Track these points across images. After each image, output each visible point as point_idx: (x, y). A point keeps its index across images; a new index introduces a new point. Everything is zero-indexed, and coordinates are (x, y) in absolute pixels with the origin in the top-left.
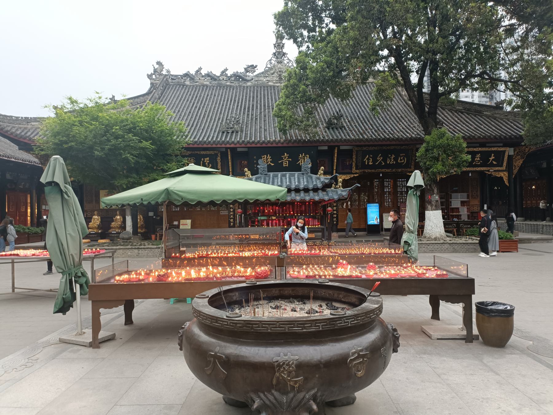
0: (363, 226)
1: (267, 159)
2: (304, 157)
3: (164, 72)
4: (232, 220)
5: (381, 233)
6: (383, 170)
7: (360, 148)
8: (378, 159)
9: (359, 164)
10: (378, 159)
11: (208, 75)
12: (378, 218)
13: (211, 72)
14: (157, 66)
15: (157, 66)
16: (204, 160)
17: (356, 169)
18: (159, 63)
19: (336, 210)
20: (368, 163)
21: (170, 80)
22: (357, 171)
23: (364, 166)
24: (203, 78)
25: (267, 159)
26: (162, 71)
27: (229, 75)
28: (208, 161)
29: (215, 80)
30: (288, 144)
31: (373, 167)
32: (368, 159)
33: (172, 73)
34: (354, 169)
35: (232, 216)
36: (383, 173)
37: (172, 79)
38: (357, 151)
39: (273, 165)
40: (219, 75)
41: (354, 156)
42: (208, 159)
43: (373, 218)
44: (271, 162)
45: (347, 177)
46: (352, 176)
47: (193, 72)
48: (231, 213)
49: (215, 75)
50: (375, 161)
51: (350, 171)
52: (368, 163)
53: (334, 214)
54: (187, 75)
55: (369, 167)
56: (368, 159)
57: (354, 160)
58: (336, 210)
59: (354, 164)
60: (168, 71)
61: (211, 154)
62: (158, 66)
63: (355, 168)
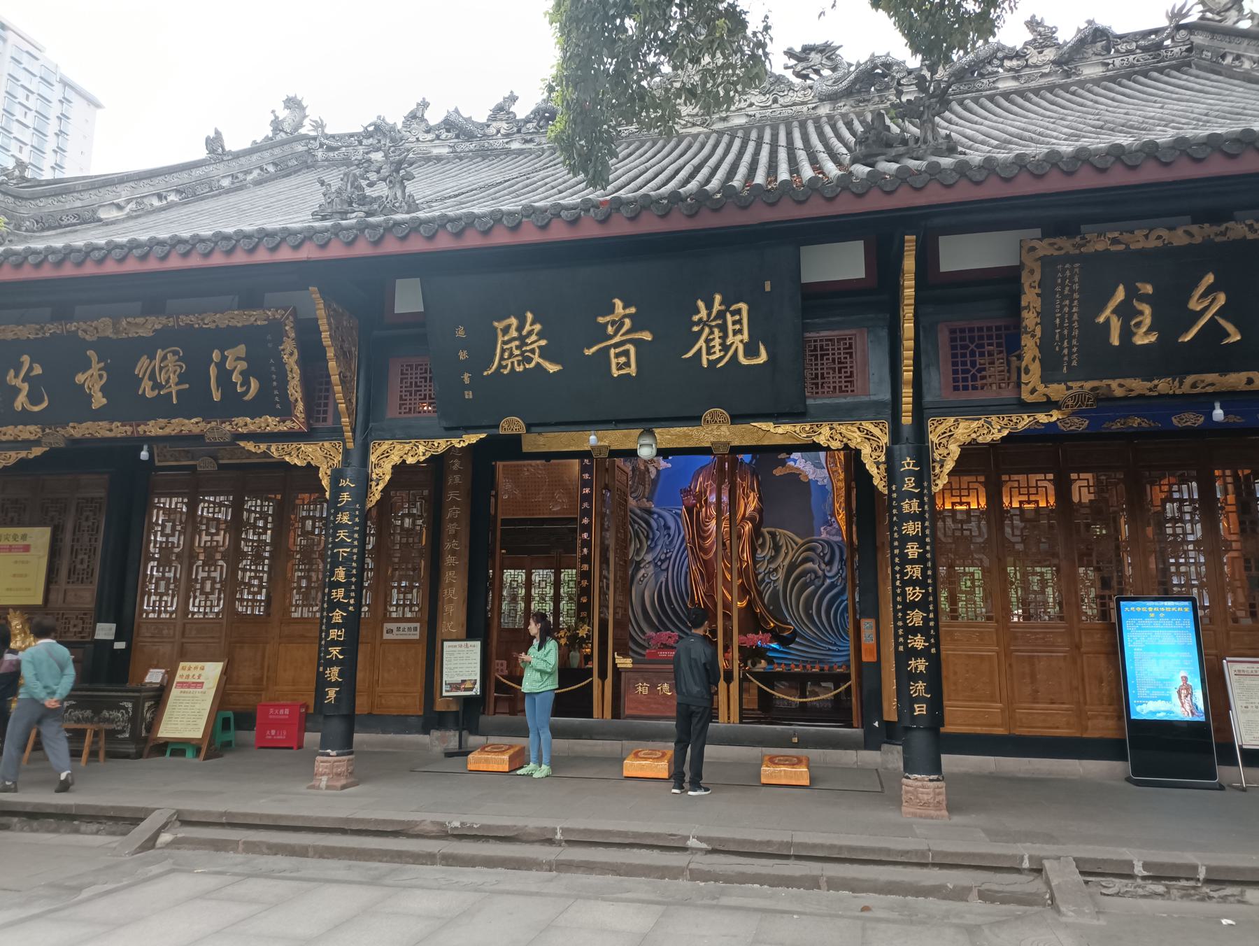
0: (1101, 727)
1: (522, 339)
2: (721, 315)
3: (306, 130)
4: (334, 673)
5: (1224, 773)
6: (1236, 380)
7: (1066, 245)
8: (1194, 305)
9: (1070, 351)
10: (1194, 305)
11: (448, 124)
12: (1196, 682)
13: (457, 111)
14: (283, 114)
15: (283, 114)
16: (224, 358)
17: (1045, 380)
18: (293, 103)
19: (923, 630)
20: (1127, 334)
21: (320, 154)
22: (1057, 391)
23: (1101, 358)
24: (430, 136)
25: (522, 339)
26: (300, 125)
27: (521, 115)
28: (243, 365)
29: (470, 137)
30: (604, 222)
31: (1167, 358)
32: (1127, 312)
33: (329, 131)
34: (1033, 377)
35: (335, 651)
36: (1229, 398)
37: (330, 149)
38: (1046, 262)
39: (552, 368)
40: (483, 120)
41: (1030, 297)
42: (241, 350)
43: (1163, 684)
44: (544, 353)
45: (994, 430)
46: (1024, 422)
47: (396, 118)
48: (334, 633)
49: (469, 120)
50: (1172, 315)
51: (1008, 394)
52: (1127, 334)
53: (915, 653)
54: (379, 130)
55: (1130, 360)
56: (1127, 312)
57: (1030, 319)
58: (923, 630)
59: (1030, 346)
60: (319, 125)
61: (252, 327)
62: (287, 112)
63: (1036, 368)
